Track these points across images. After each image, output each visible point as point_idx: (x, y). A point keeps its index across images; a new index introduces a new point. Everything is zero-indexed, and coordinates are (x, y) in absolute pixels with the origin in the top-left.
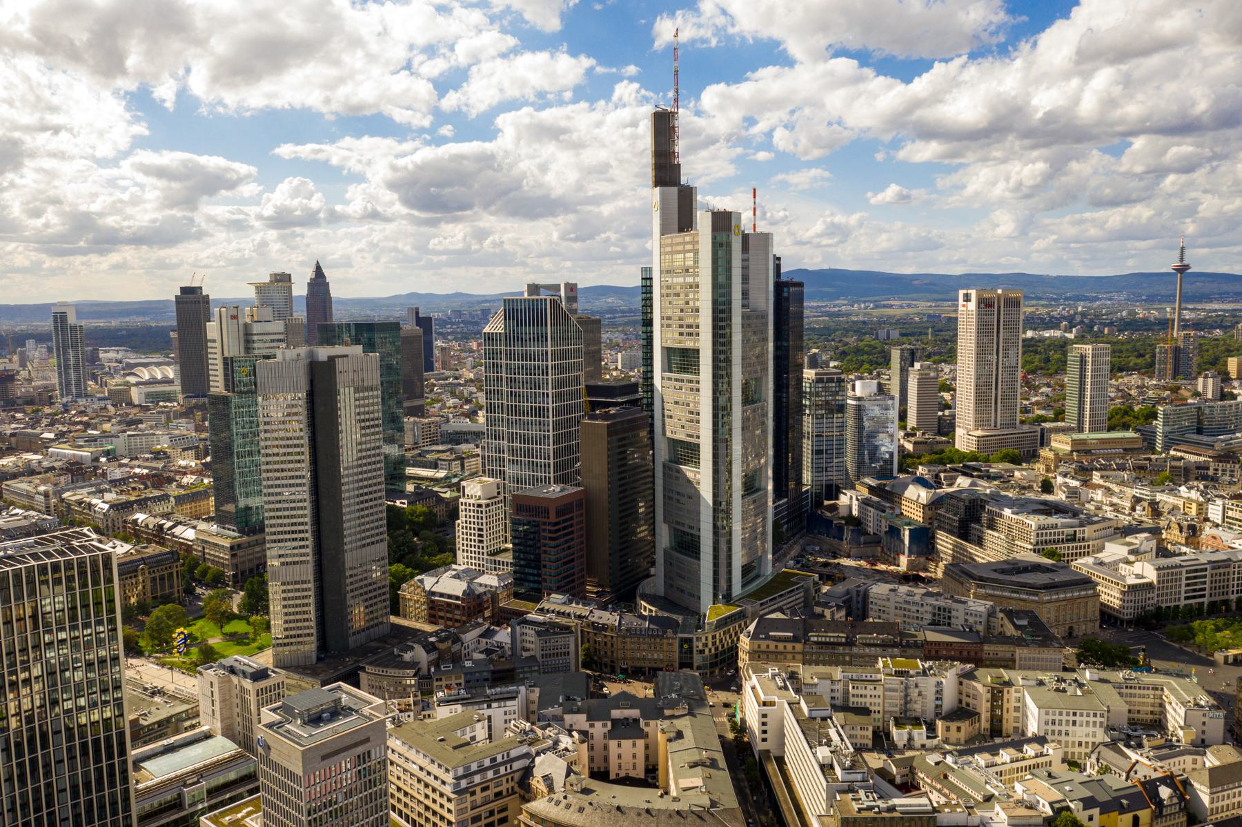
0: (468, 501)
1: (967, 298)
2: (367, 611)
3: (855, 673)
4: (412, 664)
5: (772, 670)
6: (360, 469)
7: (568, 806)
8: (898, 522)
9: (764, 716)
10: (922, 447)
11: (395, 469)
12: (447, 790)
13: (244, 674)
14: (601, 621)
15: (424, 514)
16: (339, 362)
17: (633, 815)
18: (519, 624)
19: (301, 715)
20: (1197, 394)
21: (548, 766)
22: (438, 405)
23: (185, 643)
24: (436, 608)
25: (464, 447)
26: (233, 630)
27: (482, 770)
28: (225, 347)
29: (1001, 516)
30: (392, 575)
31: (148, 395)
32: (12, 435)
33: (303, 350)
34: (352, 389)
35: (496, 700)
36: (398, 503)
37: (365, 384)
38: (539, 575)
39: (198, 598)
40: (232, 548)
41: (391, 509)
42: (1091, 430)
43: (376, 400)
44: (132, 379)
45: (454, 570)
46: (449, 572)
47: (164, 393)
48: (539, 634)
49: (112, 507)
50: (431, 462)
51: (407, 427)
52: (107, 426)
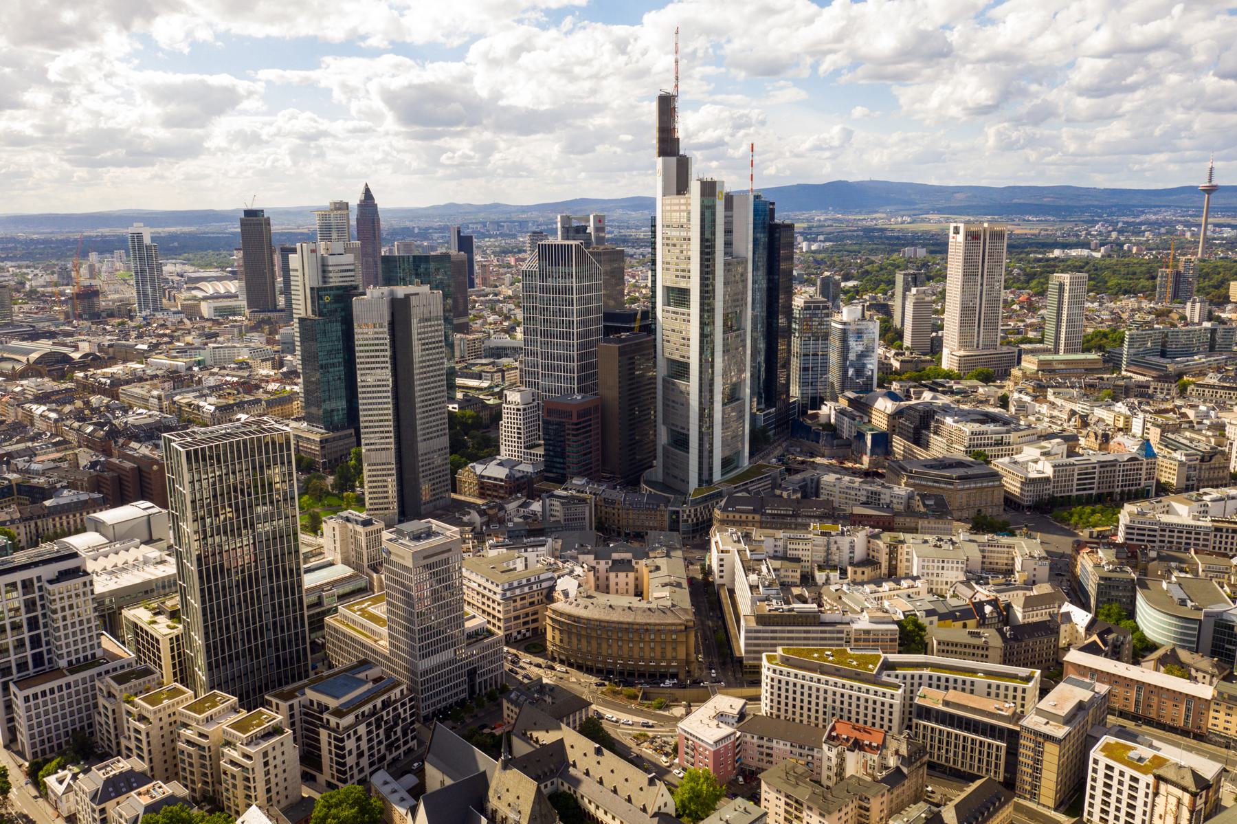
1: (957, 231)
3: (791, 534)
5: (732, 530)
7: (578, 605)
8: (864, 428)
9: (722, 560)
10: (909, 365)
12: (498, 598)
13: (357, 521)
15: (472, 417)
16: (412, 298)
17: (620, 610)
19: (408, 534)
20: (1183, 318)
21: (566, 584)
22: (479, 322)
24: (485, 488)
25: (505, 361)
27: (521, 586)
29: (943, 423)
31: (216, 309)
32: (110, 346)
33: (386, 289)
40: (321, 441)
42: (1066, 352)
48: (562, 504)
49: (217, 408)
52: (189, 339)
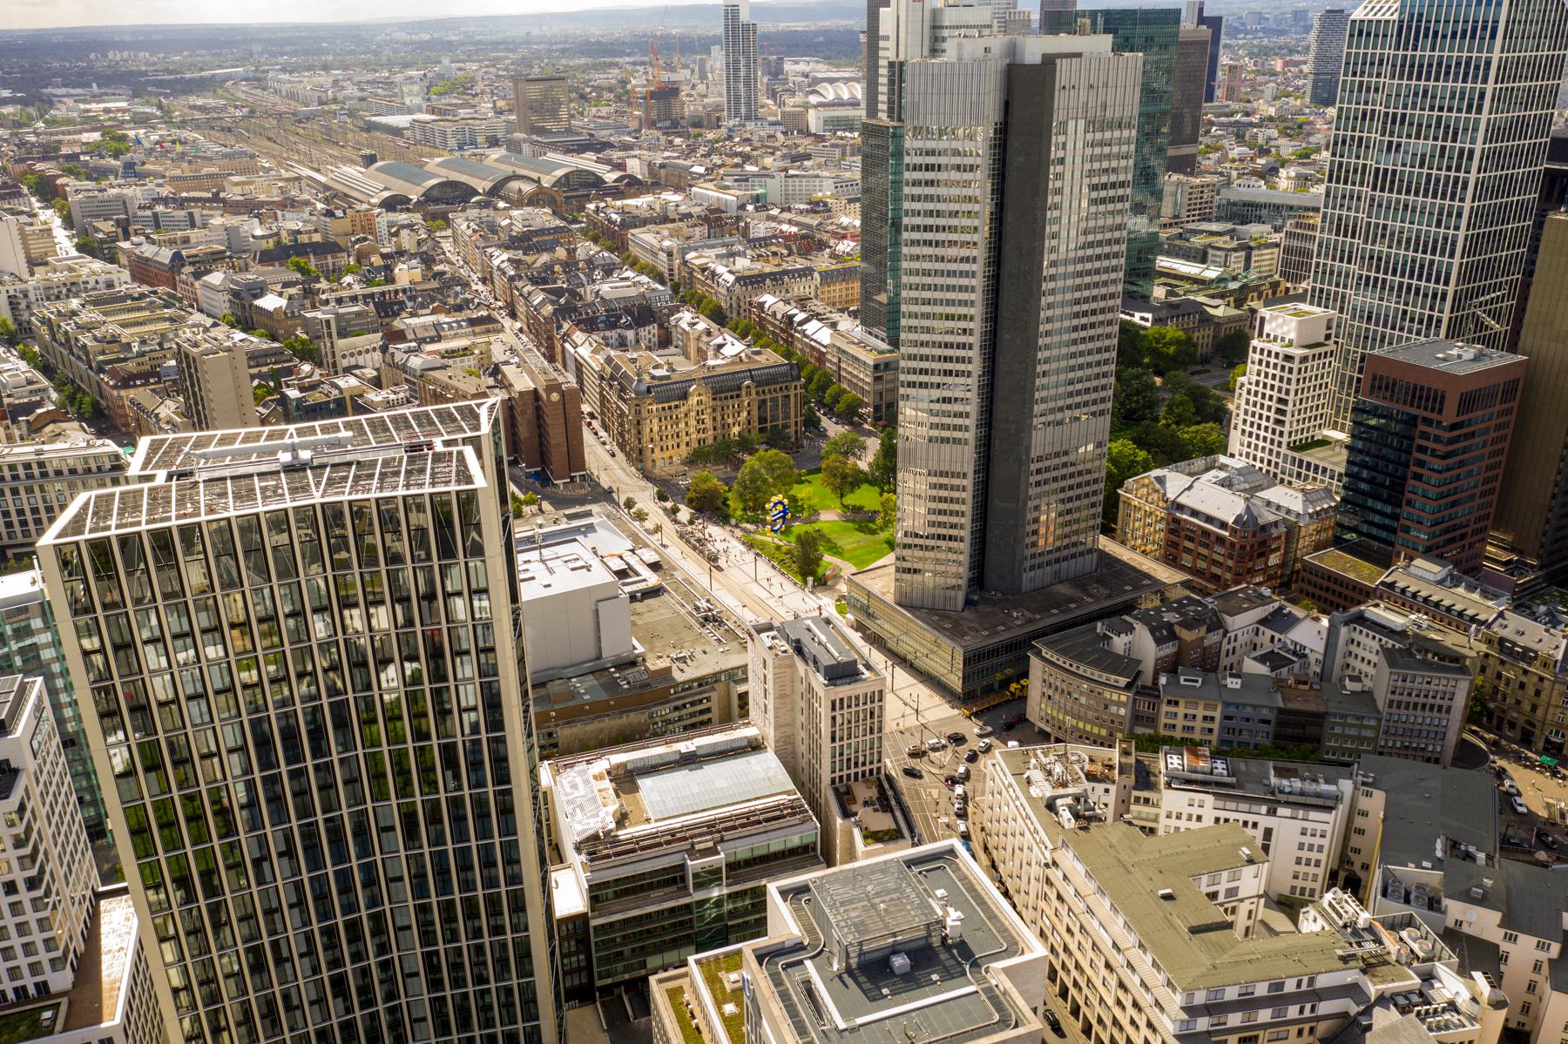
0: (1267, 346)
2: (1060, 520)
4: (1127, 665)
6: (1078, 281)
11: (1139, 259)
14: (1521, 641)
15: (1178, 342)
16: (1063, 69)
18: (1346, 624)
22: (1215, 156)
23: (783, 517)
25: (1254, 229)
26: (858, 503)
28: (902, 48)
30: (1113, 461)
32: (662, 166)
34: (1081, 123)
35: (1287, 804)
36: (1137, 318)
37: (1109, 114)
38: (1395, 517)
39: (823, 435)
40: (876, 367)
41: (1127, 330)
43: (1124, 148)
44: (814, 99)
45: (1223, 467)
46: (1214, 472)
47: (847, 119)
48: (1389, 654)
49: (738, 280)
50: (1197, 250)
51: (1168, 189)
52: (768, 161)
